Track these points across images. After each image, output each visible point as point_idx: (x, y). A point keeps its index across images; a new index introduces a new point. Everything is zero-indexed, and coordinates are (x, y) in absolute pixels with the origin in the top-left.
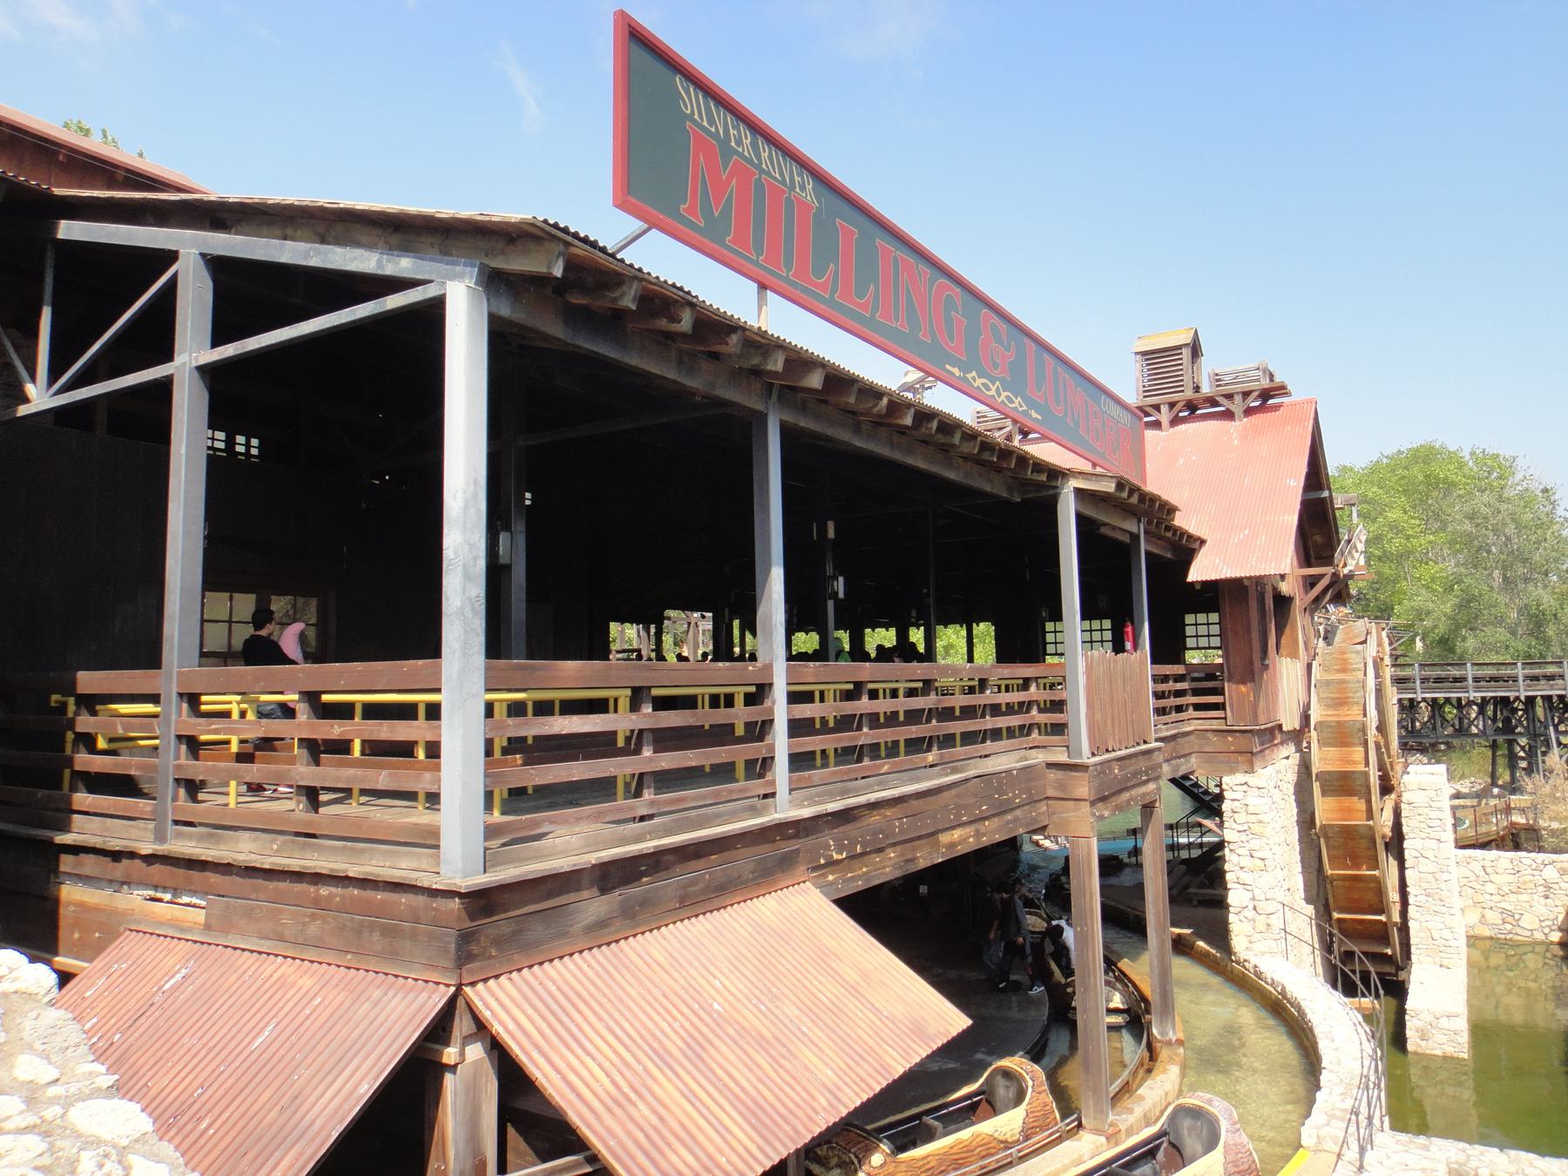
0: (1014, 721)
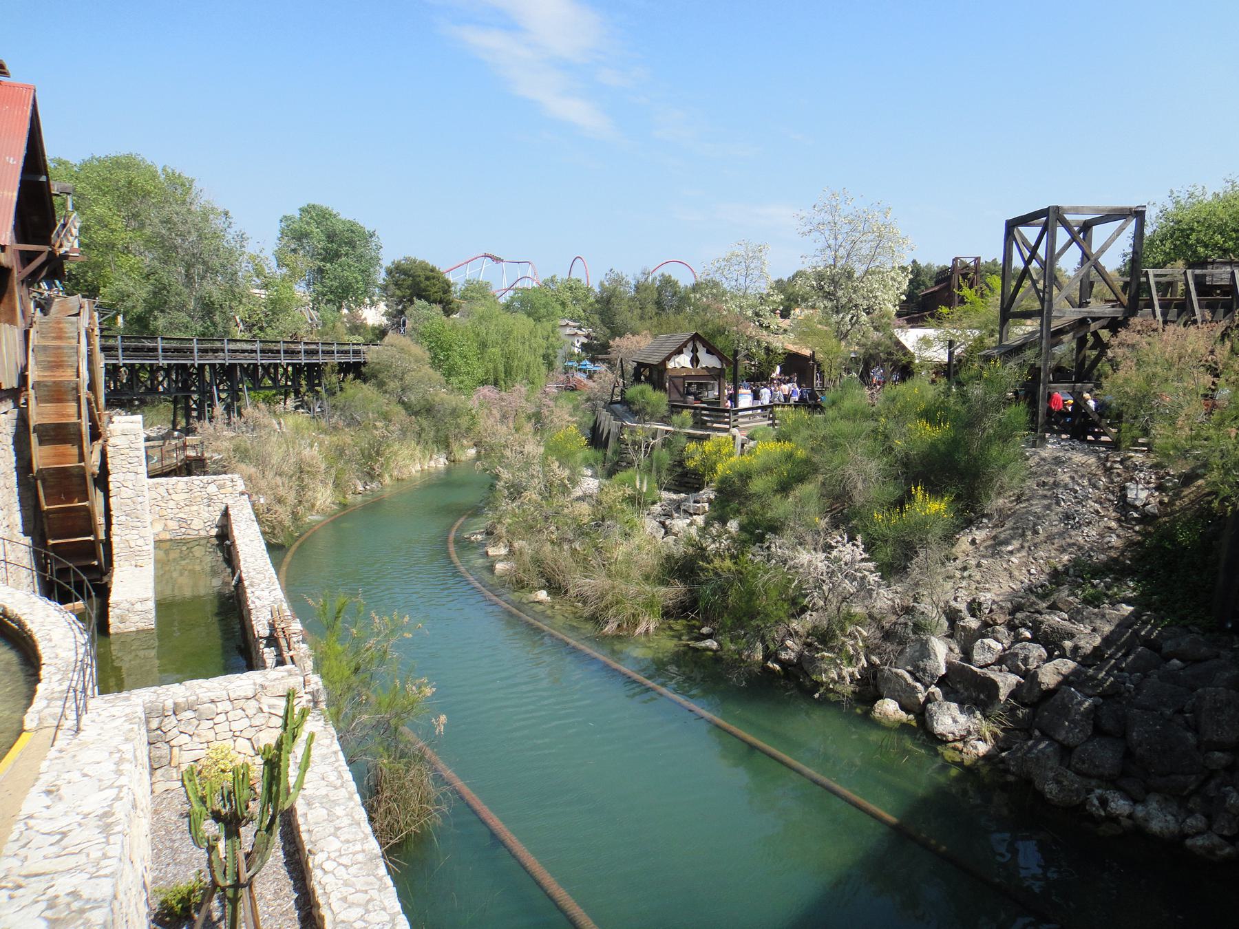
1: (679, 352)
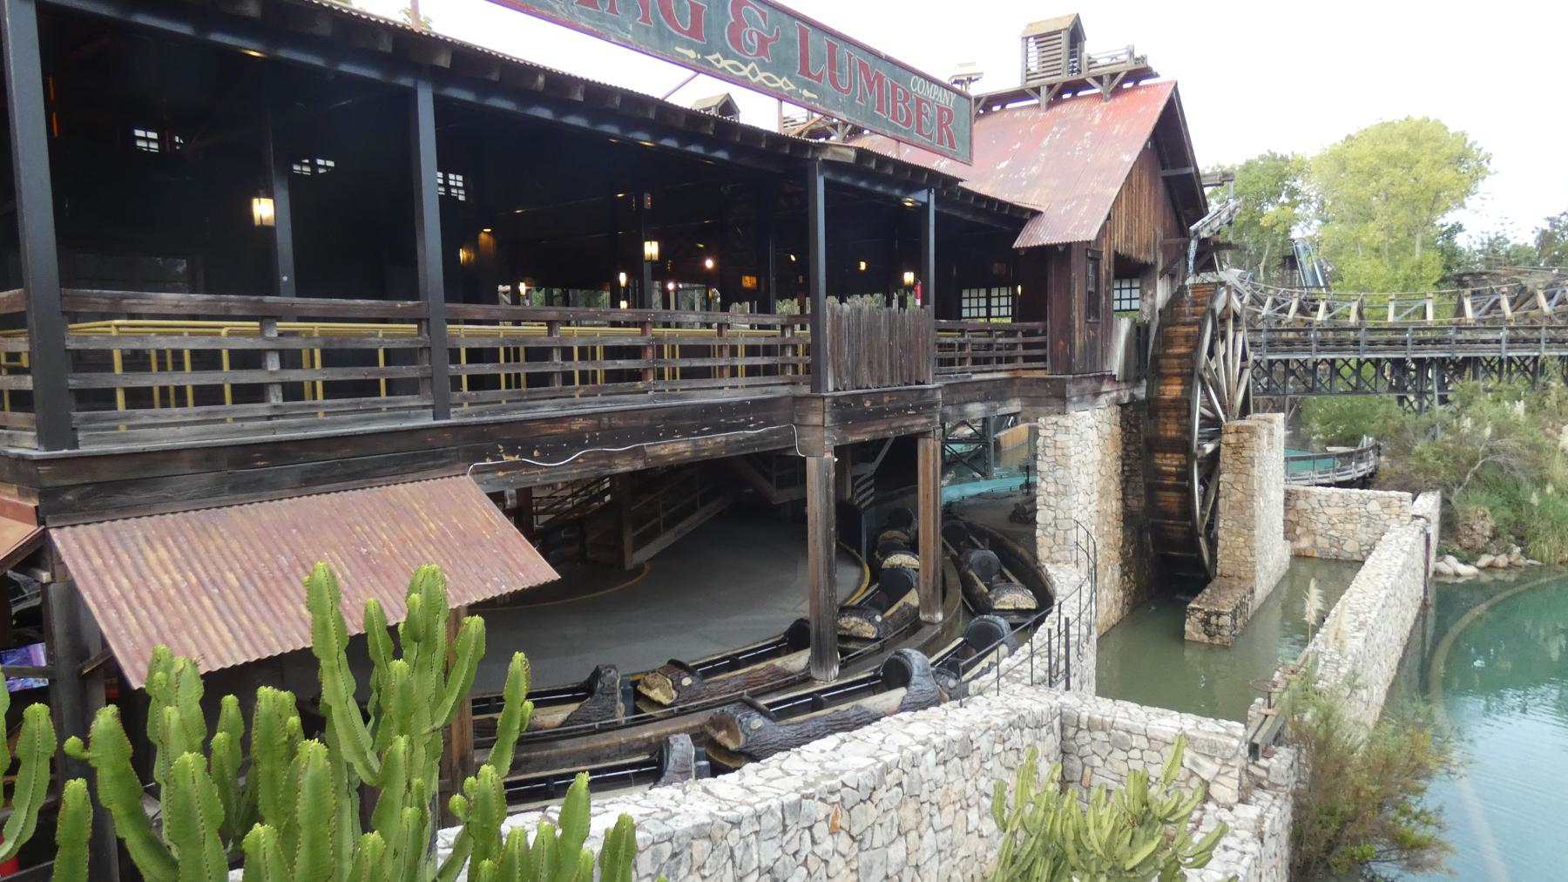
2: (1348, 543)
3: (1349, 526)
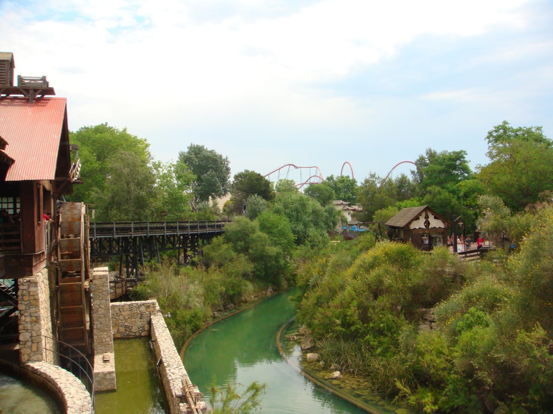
0: (155, 225)
1: (417, 218)
2: (133, 328)
3: (133, 320)
